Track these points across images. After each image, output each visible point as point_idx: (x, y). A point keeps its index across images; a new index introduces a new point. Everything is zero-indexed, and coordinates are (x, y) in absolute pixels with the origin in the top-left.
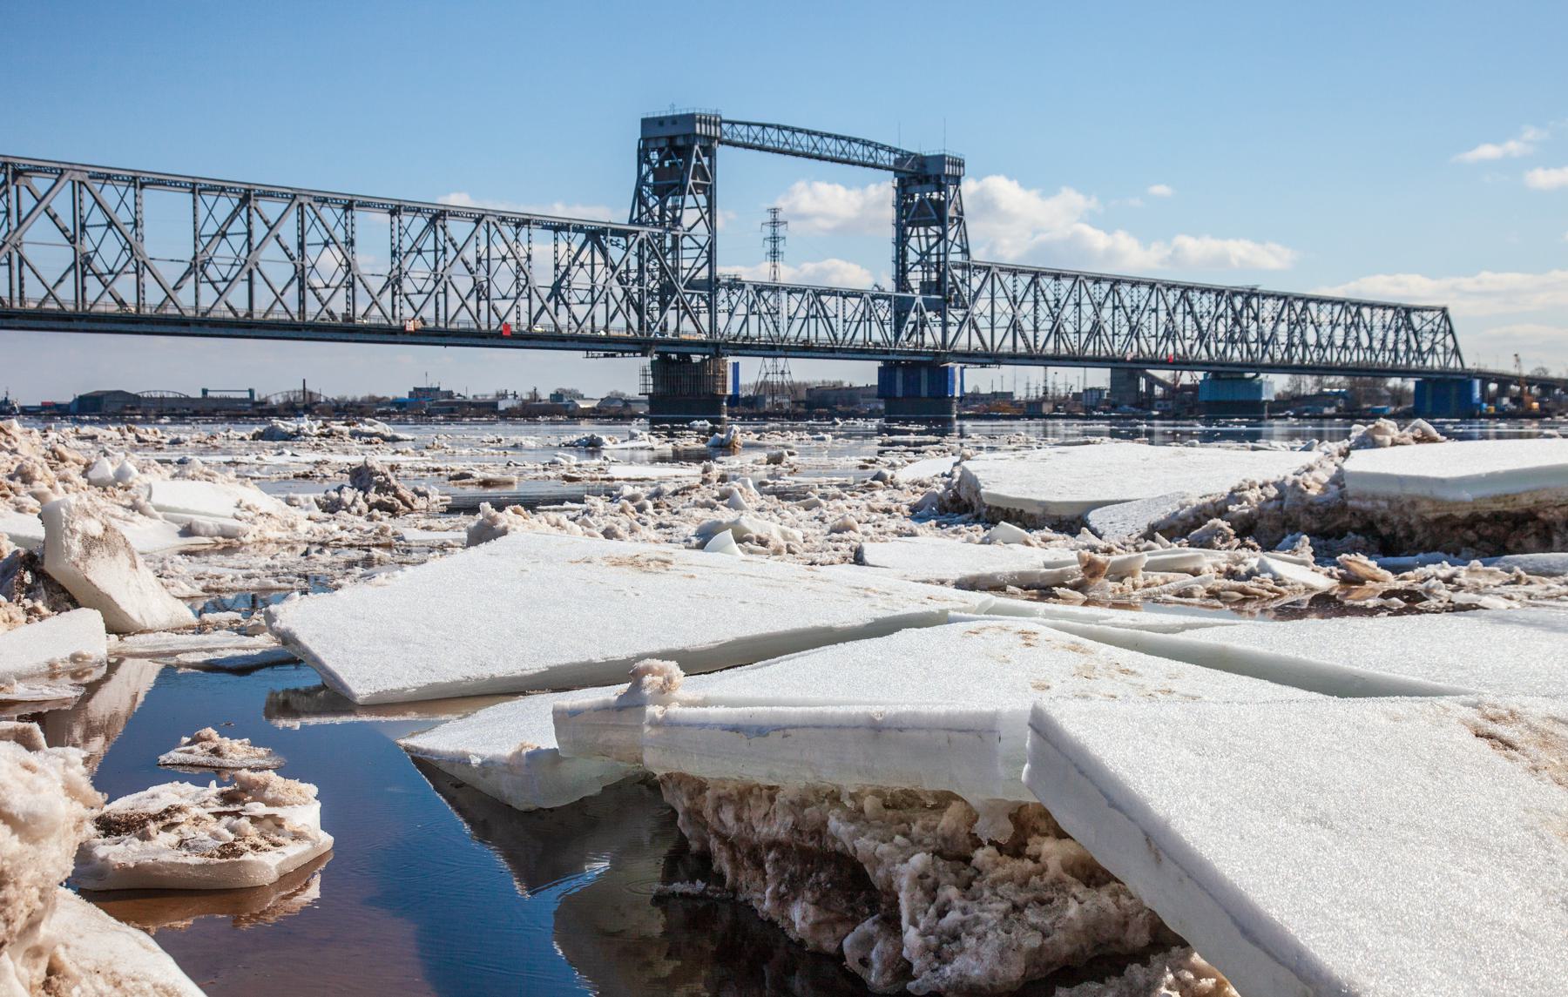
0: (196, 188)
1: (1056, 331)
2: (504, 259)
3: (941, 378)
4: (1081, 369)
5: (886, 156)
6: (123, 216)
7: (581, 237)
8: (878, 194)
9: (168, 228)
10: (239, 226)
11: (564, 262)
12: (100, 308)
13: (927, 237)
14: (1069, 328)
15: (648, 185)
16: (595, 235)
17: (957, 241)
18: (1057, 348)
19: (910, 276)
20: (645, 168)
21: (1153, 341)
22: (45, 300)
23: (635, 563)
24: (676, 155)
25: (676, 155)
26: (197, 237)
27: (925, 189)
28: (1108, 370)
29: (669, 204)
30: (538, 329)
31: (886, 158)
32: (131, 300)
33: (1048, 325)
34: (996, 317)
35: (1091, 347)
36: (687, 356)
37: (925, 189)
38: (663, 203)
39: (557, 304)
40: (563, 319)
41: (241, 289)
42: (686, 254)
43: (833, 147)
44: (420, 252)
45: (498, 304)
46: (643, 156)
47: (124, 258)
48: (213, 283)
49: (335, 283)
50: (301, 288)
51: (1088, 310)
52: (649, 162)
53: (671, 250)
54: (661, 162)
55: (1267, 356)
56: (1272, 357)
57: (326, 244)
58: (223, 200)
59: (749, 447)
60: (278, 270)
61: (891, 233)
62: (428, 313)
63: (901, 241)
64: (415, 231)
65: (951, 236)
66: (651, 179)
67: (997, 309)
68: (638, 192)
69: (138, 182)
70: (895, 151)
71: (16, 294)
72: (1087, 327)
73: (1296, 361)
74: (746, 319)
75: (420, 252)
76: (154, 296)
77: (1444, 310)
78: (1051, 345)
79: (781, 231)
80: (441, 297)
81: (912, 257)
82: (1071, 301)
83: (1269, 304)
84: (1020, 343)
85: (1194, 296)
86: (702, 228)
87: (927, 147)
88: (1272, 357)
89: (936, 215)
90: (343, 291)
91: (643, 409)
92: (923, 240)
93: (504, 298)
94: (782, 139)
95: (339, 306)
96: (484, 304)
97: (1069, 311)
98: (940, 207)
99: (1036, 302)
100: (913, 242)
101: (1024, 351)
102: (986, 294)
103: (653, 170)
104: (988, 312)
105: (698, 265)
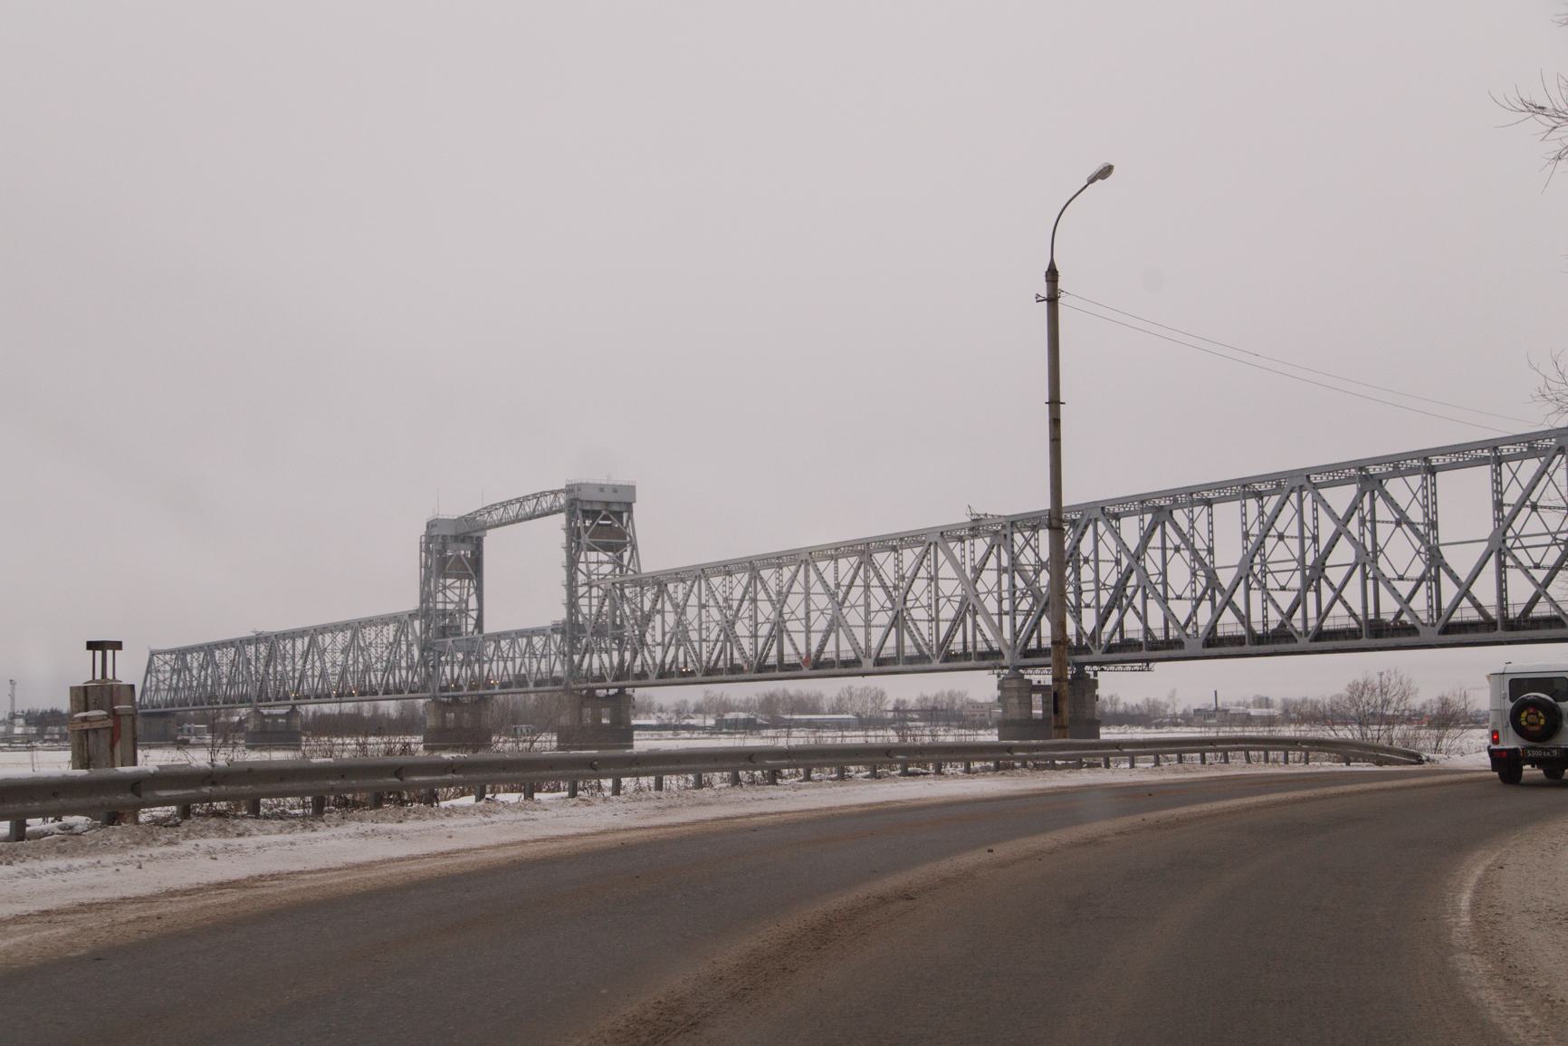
1: (899, 621)
3: (621, 703)
6: (1416, 514)
11: (1255, 530)
12: (1456, 617)
14: (920, 614)
18: (900, 644)
21: (659, 650)
22: (1400, 613)
23: (364, 835)
30: (1328, 624)
35: (959, 637)
36: (592, 691)
39: (1145, 597)
45: (1276, 595)
48: (1526, 571)
50: (1501, 566)
55: (1228, 617)
56: (1244, 619)
57: (1398, 524)
59: (791, 775)
61: (562, 556)
63: (572, 564)
73: (1514, 611)
76: (1520, 591)
77: (153, 654)
81: (581, 578)
82: (923, 572)
83: (1228, 516)
87: (597, 472)
88: (1244, 619)
93: (1283, 589)
96: (1256, 597)
98: (622, 535)
99: (867, 587)
101: (914, 651)
104: (801, 613)
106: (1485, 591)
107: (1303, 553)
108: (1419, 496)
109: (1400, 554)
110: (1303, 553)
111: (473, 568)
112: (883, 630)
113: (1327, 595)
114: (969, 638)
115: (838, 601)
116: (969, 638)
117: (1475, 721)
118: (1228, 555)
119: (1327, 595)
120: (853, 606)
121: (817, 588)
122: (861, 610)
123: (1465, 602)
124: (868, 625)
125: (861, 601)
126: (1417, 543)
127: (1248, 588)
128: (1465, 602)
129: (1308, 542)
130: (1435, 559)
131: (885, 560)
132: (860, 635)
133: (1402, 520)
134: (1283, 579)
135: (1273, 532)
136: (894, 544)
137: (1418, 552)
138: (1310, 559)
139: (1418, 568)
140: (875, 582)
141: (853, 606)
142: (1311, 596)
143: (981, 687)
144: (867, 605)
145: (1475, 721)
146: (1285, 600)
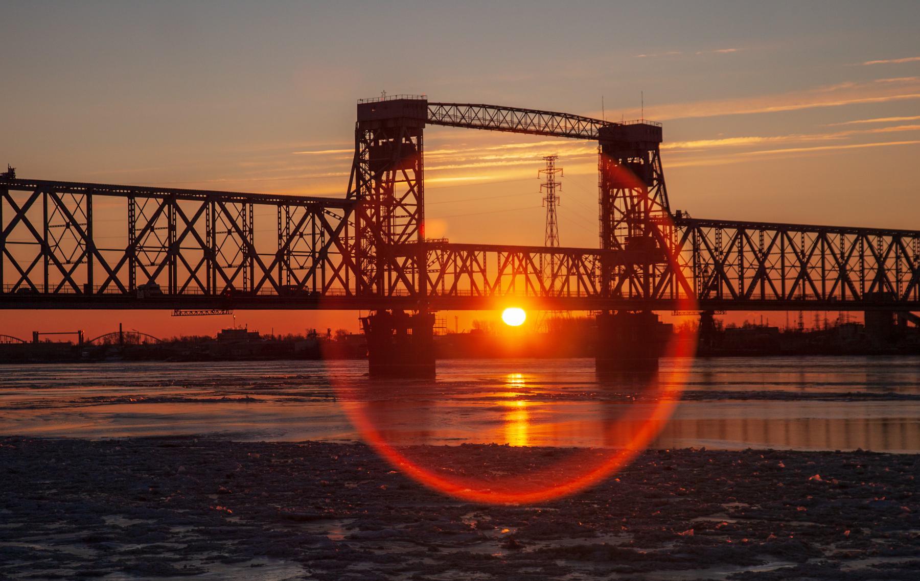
0: (132, 192)
1: (843, 276)
2: (229, 232)
4: (784, 312)
5: (588, 127)
6: (80, 218)
7: (302, 210)
8: (582, 162)
9: (111, 220)
10: (162, 221)
13: (632, 197)
15: (365, 162)
16: (316, 206)
17: (658, 200)
19: (617, 232)
20: (362, 147)
24: (392, 132)
25: (392, 132)
26: (131, 230)
27: (629, 150)
28: (863, 312)
29: (384, 178)
31: (596, 128)
32: (125, 282)
33: (834, 275)
34: (787, 269)
37: (629, 150)
38: (378, 178)
40: (56, 277)
41: (83, 268)
42: (399, 221)
43: (563, 124)
44: (301, 235)
46: (359, 136)
47: (79, 252)
49: (75, 259)
51: (870, 261)
52: (365, 141)
53: (384, 217)
54: (376, 140)
57: (68, 226)
58: (152, 201)
60: (192, 254)
61: (595, 193)
62: (238, 284)
64: (296, 219)
65: (651, 195)
66: (367, 157)
67: (787, 263)
68: (356, 166)
69: (90, 190)
70: (598, 122)
71: (211, 285)
72: (750, 273)
74: (567, 280)
75: (301, 235)
76: (141, 279)
78: (757, 291)
79: (557, 193)
80: (249, 269)
84: (848, 292)
85: (906, 240)
86: (411, 199)
87: (627, 116)
89: (649, 176)
90: (166, 267)
91: (691, 343)
92: (628, 200)
94: (516, 120)
95: (80, 277)
97: (854, 262)
98: (649, 168)
100: (619, 203)
101: (852, 299)
102: (776, 249)
103: (368, 146)
104: (778, 265)
105: (409, 230)
106: (123, 276)
107: (314, 244)
108: (137, 211)
109: (229, 250)
110: (314, 244)
111: (411, 157)
112: (834, 282)
113: (329, 273)
114: (674, 291)
115: (880, 260)
116: (674, 291)
117: (817, 316)
118: (266, 243)
119: (329, 273)
120: (730, 265)
121: (868, 252)
122: (820, 270)
123: (112, 283)
124: (741, 278)
125: (820, 264)
126: (79, 237)
127: (281, 269)
128: (112, 283)
129: (317, 237)
130: (91, 250)
131: (754, 235)
132: (778, 285)
133: (72, 222)
134: (301, 260)
135: (233, 229)
136: (762, 227)
137: (219, 250)
138: (318, 247)
139: (239, 260)
140: (828, 252)
141: (730, 265)
142: (319, 272)
143: (858, 317)
144: (741, 265)
145: (817, 316)
146: (301, 275)
